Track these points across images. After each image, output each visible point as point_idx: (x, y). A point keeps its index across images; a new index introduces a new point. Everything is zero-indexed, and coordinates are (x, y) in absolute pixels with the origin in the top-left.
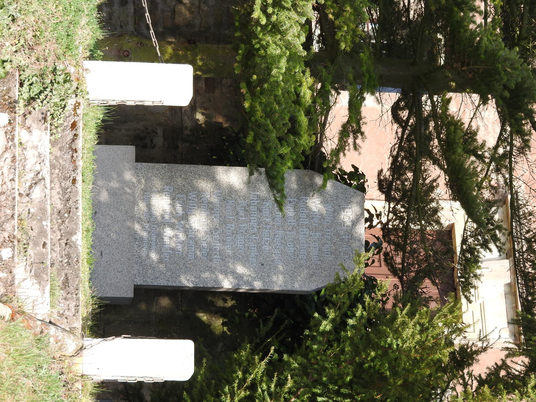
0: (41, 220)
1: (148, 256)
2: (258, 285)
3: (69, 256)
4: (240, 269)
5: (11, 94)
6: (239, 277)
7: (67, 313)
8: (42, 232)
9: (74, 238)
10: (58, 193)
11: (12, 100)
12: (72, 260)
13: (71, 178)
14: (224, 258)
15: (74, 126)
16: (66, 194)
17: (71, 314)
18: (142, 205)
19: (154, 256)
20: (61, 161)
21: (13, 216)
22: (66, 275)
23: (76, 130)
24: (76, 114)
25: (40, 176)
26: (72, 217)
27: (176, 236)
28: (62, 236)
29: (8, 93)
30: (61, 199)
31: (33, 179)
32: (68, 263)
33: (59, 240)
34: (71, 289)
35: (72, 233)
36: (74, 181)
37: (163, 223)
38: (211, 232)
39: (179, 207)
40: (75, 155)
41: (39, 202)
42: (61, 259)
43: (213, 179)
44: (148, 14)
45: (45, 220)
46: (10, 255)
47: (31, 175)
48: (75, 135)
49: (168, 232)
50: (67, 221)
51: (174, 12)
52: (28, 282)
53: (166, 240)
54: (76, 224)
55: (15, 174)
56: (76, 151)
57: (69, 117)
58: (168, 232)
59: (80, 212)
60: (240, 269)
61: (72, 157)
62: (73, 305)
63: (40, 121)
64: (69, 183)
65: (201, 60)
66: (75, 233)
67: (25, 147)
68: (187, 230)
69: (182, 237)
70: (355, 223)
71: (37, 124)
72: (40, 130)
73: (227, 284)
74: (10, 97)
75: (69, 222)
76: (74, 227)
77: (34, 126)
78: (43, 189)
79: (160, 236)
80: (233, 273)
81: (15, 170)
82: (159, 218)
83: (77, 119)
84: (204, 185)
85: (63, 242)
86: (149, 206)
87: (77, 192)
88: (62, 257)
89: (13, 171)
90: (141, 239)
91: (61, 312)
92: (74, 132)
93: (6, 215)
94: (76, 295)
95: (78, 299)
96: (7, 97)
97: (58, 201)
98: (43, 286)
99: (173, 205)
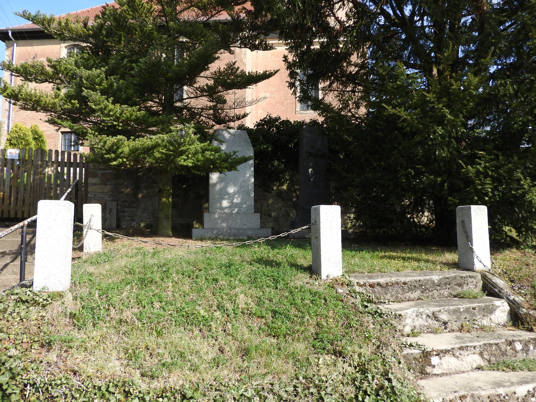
0: (460, 312)
1: (244, 208)
2: (252, 169)
3: (446, 284)
4: (248, 175)
5: (418, 356)
6: (250, 176)
7: (474, 283)
8: (467, 310)
9: (436, 282)
10: (412, 293)
11: (422, 355)
12: (448, 282)
13: (403, 285)
14: (244, 181)
15: (372, 286)
16: (412, 288)
17: (475, 280)
18: (226, 211)
19: (244, 206)
20: (393, 293)
21: (496, 344)
22: (455, 285)
23: (375, 284)
24: (365, 285)
25: (430, 315)
26: (425, 284)
27: (236, 198)
28: (435, 289)
29: (417, 359)
30: (415, 292)
31: (432, 319)
32: (449, 284)
33: (437, 291)
34: (462, 281)
35: (433, 282)
36: (405, 283)
37: (232, 203)
38: (235, 185)
39: (226, 197)
40: (390, 284)
41: (449, 315)
42: (448, 289)
43: (215, 185)
44: (281, 235)
45: (460, 310)
46: (519, 343)
47: (430, 321)
48: (378, 285)
49: (235, 200)
50: (427, 286)
51: (127, 195)
52: (493, 316)
53: (238, 201)
54: (428, 280)
55: (471, 346)
56: (387, 284)
57: (367, 290)
58: (235, 200)
59: (422, 278)
60: (248, 175)
61: (390, 286)
62: (470, 280)
63: (400, 319)
64: (406, 287)
65: (167, 187)
66: (434, 281)
67: (413, 327)
68: (235, 193)
69: (237, 196)
70: (229, 133)
71: (402, 321)
72: (406, 319)
73: (253, 180)
74: (421, 357)
75: (428, 285)
76: (430, 281)
77: (403, 323)
78: (442, 313)
79: (236, 204)
80: (249, 178)
81: (468, 346)
82: (230, 204)
83: (367, 284)
84: (218, 187)
85: (439, 288)
86: (226, 208)
87: (411, 281)
88: (446, 288)
89: (469, 348)
90: (238, 211)
91: (474, 286)
92: (376, 286)
93: (496, 350)
94: (465, 278)
95: (467, 277)
96: (420, 360)
97: (417, 293)
98: (496, 307)
99: (225, 199)
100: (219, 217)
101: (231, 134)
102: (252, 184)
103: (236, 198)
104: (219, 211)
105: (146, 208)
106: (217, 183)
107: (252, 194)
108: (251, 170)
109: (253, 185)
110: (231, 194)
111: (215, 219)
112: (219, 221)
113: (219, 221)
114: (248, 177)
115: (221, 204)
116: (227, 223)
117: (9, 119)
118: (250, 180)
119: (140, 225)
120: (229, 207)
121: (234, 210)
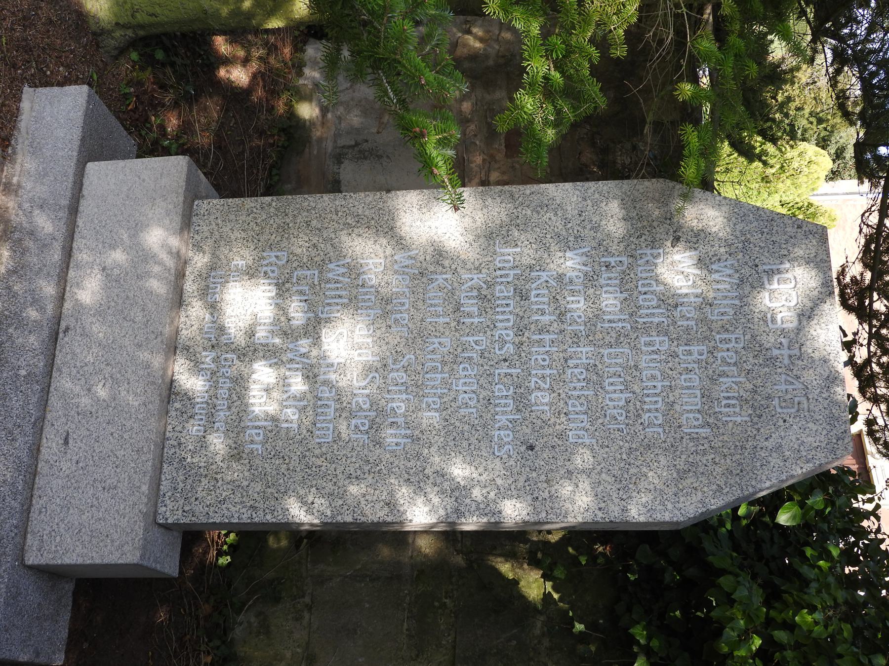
1: (202, 443)
4: (460, 471)
27: (284, 383)
60: (460, 471)
69: (298, 385)
79: (240, 383)
86: (214, 307)
90: (187, 398)
100: (143, 256)
101: (799, 330)
102: (391, 505)
103: (284, 383)
104: (200, 261)
105: (386, 118)
106: (399, 242)
107: (309, 507)
108: (504, 494)
109: (374, 514)
110: (317, 341)
111: (138, 227)
112: (118, 256)
113: (118, 256)
114: (441, 474)
115: (251, 273)
116: (100, 312)
117: (844, 194)
118: (419, 489)
119: (308, 98)
120: (221, 329)
121: (197, 367)
